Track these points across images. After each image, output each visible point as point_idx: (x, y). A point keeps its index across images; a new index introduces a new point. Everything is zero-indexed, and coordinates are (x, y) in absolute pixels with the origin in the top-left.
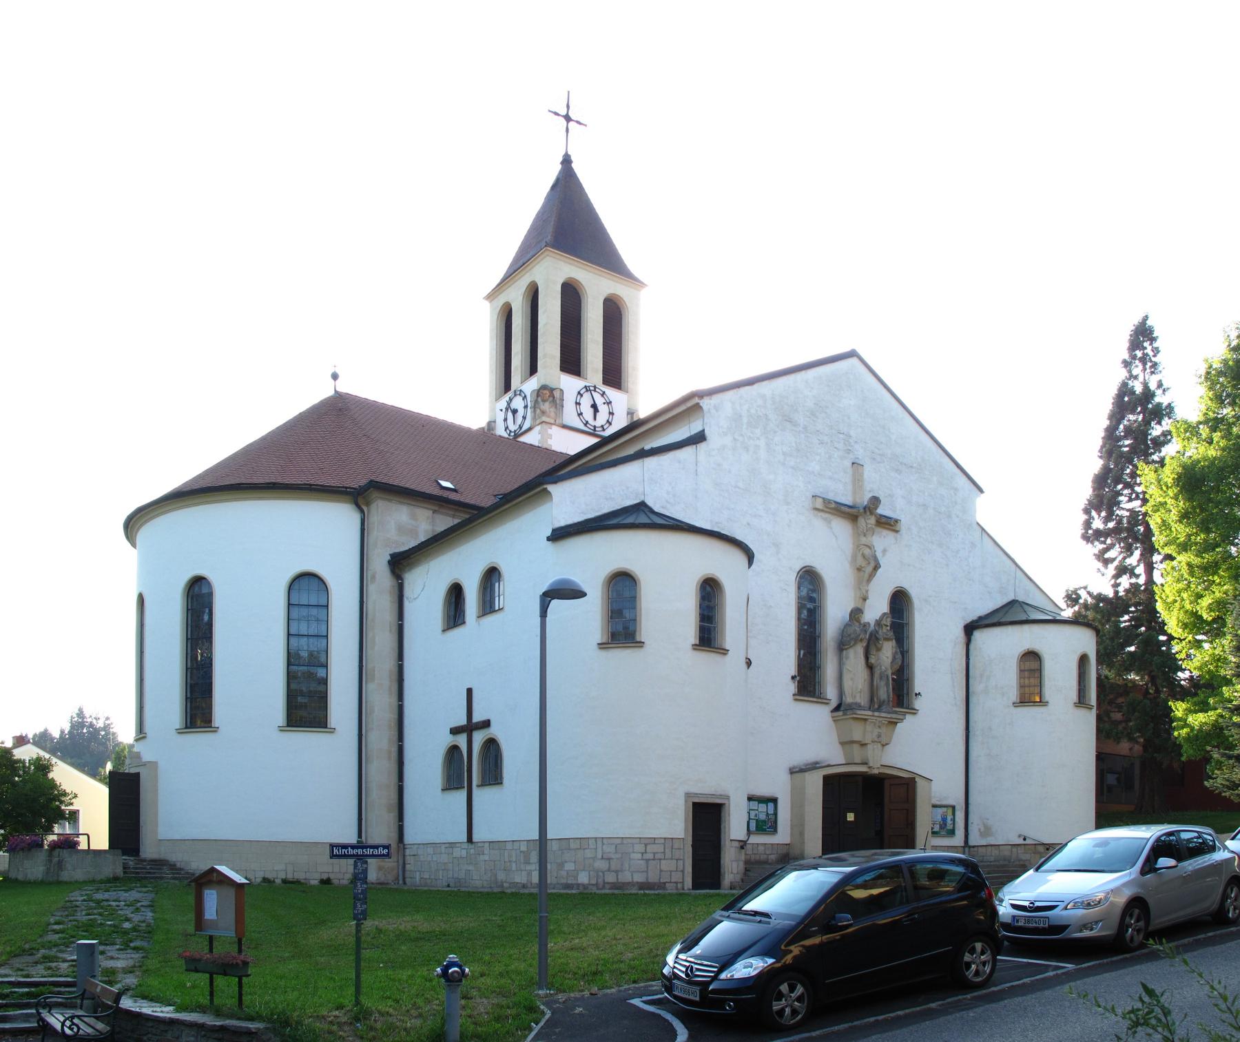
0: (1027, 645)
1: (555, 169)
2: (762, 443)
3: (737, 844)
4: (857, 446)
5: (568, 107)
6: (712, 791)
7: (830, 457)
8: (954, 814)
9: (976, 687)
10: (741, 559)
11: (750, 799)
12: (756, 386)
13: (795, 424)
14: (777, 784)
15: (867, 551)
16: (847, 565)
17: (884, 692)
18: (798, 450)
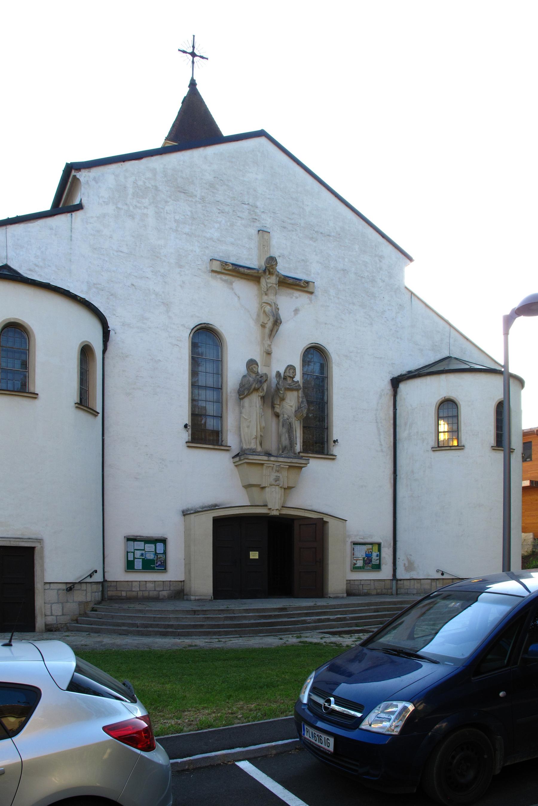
0: (444, 394)
1: (185, 91)
2: (151, 211)
3: (64, 587)
4: (263, 216)
5: (193, 47)
6: (18, 534)
7: (232, 225)
8: (379, 550)
9: (402, 434)
12: (144, 161)
13: (192, 196)
14: (171, 527)
15: (268, 308)
16: (252, 323)
18: (194, 219)
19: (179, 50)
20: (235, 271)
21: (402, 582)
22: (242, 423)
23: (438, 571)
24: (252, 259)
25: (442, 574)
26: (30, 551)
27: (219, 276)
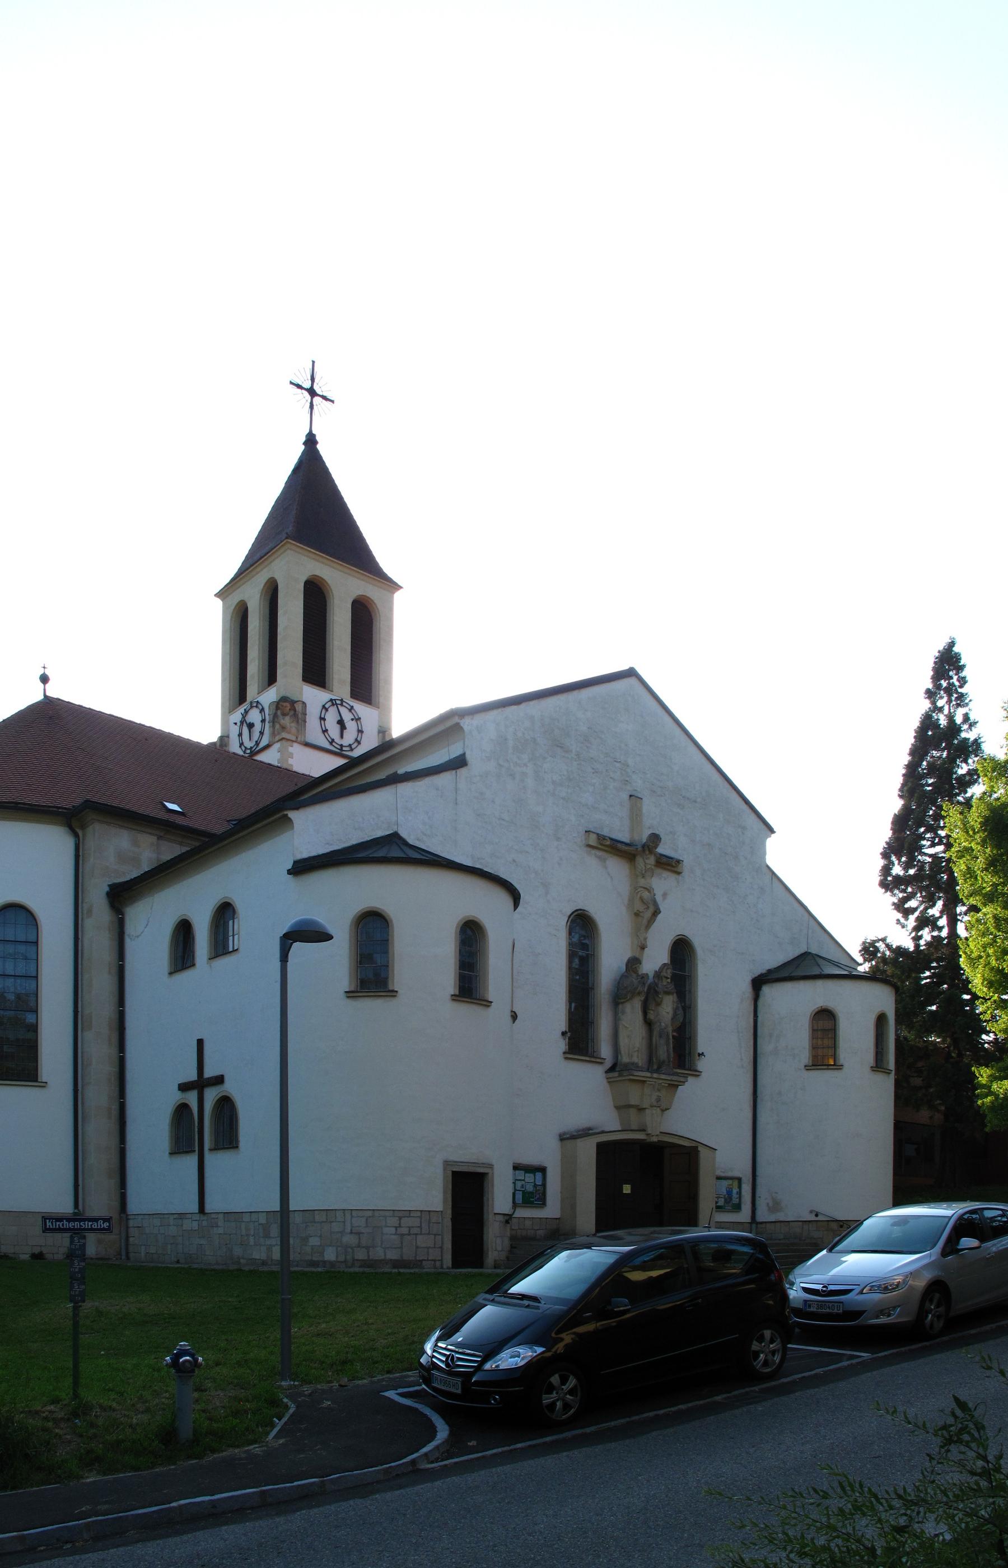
0: (820, 1003)
1: (298, 449)
5: (313, 379)
8: (740, 1187)
9: (766, 1047)
10: (504, 899)
11: (516, 1167)
12: (523, 706)
14: (546, 1152)
17: (665, 1051)
19: (291, 383)
20: (610, 847)
21: (763, 1226)
22: (622, 1031)
23: (811, 1212)
24: (620, 831)
25: (817, 1215)
26: (455, 1174)
27: (593, 851)
